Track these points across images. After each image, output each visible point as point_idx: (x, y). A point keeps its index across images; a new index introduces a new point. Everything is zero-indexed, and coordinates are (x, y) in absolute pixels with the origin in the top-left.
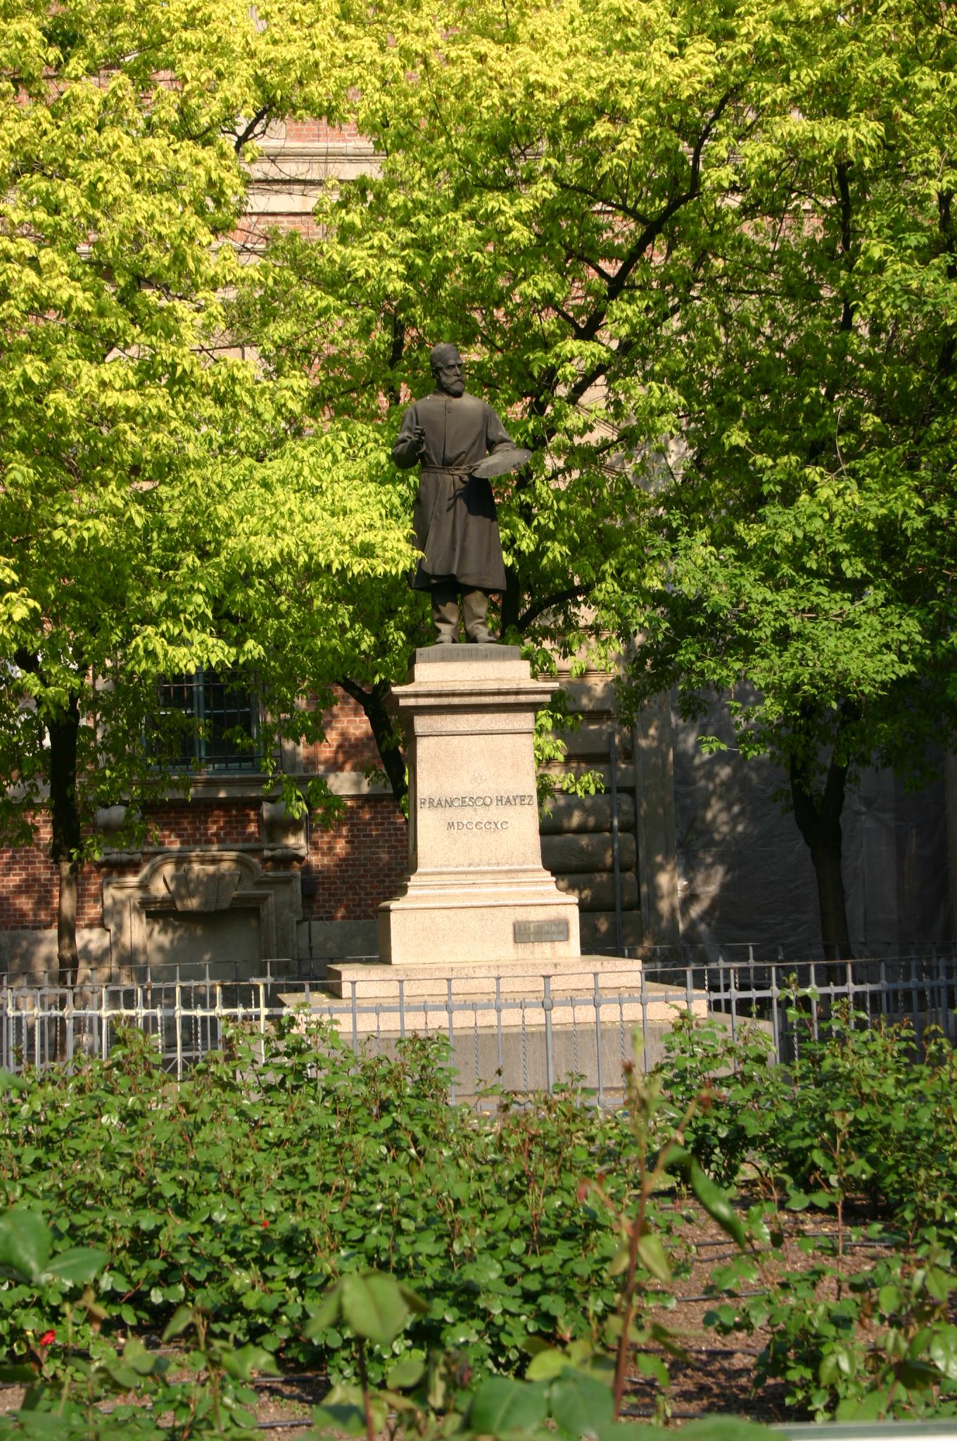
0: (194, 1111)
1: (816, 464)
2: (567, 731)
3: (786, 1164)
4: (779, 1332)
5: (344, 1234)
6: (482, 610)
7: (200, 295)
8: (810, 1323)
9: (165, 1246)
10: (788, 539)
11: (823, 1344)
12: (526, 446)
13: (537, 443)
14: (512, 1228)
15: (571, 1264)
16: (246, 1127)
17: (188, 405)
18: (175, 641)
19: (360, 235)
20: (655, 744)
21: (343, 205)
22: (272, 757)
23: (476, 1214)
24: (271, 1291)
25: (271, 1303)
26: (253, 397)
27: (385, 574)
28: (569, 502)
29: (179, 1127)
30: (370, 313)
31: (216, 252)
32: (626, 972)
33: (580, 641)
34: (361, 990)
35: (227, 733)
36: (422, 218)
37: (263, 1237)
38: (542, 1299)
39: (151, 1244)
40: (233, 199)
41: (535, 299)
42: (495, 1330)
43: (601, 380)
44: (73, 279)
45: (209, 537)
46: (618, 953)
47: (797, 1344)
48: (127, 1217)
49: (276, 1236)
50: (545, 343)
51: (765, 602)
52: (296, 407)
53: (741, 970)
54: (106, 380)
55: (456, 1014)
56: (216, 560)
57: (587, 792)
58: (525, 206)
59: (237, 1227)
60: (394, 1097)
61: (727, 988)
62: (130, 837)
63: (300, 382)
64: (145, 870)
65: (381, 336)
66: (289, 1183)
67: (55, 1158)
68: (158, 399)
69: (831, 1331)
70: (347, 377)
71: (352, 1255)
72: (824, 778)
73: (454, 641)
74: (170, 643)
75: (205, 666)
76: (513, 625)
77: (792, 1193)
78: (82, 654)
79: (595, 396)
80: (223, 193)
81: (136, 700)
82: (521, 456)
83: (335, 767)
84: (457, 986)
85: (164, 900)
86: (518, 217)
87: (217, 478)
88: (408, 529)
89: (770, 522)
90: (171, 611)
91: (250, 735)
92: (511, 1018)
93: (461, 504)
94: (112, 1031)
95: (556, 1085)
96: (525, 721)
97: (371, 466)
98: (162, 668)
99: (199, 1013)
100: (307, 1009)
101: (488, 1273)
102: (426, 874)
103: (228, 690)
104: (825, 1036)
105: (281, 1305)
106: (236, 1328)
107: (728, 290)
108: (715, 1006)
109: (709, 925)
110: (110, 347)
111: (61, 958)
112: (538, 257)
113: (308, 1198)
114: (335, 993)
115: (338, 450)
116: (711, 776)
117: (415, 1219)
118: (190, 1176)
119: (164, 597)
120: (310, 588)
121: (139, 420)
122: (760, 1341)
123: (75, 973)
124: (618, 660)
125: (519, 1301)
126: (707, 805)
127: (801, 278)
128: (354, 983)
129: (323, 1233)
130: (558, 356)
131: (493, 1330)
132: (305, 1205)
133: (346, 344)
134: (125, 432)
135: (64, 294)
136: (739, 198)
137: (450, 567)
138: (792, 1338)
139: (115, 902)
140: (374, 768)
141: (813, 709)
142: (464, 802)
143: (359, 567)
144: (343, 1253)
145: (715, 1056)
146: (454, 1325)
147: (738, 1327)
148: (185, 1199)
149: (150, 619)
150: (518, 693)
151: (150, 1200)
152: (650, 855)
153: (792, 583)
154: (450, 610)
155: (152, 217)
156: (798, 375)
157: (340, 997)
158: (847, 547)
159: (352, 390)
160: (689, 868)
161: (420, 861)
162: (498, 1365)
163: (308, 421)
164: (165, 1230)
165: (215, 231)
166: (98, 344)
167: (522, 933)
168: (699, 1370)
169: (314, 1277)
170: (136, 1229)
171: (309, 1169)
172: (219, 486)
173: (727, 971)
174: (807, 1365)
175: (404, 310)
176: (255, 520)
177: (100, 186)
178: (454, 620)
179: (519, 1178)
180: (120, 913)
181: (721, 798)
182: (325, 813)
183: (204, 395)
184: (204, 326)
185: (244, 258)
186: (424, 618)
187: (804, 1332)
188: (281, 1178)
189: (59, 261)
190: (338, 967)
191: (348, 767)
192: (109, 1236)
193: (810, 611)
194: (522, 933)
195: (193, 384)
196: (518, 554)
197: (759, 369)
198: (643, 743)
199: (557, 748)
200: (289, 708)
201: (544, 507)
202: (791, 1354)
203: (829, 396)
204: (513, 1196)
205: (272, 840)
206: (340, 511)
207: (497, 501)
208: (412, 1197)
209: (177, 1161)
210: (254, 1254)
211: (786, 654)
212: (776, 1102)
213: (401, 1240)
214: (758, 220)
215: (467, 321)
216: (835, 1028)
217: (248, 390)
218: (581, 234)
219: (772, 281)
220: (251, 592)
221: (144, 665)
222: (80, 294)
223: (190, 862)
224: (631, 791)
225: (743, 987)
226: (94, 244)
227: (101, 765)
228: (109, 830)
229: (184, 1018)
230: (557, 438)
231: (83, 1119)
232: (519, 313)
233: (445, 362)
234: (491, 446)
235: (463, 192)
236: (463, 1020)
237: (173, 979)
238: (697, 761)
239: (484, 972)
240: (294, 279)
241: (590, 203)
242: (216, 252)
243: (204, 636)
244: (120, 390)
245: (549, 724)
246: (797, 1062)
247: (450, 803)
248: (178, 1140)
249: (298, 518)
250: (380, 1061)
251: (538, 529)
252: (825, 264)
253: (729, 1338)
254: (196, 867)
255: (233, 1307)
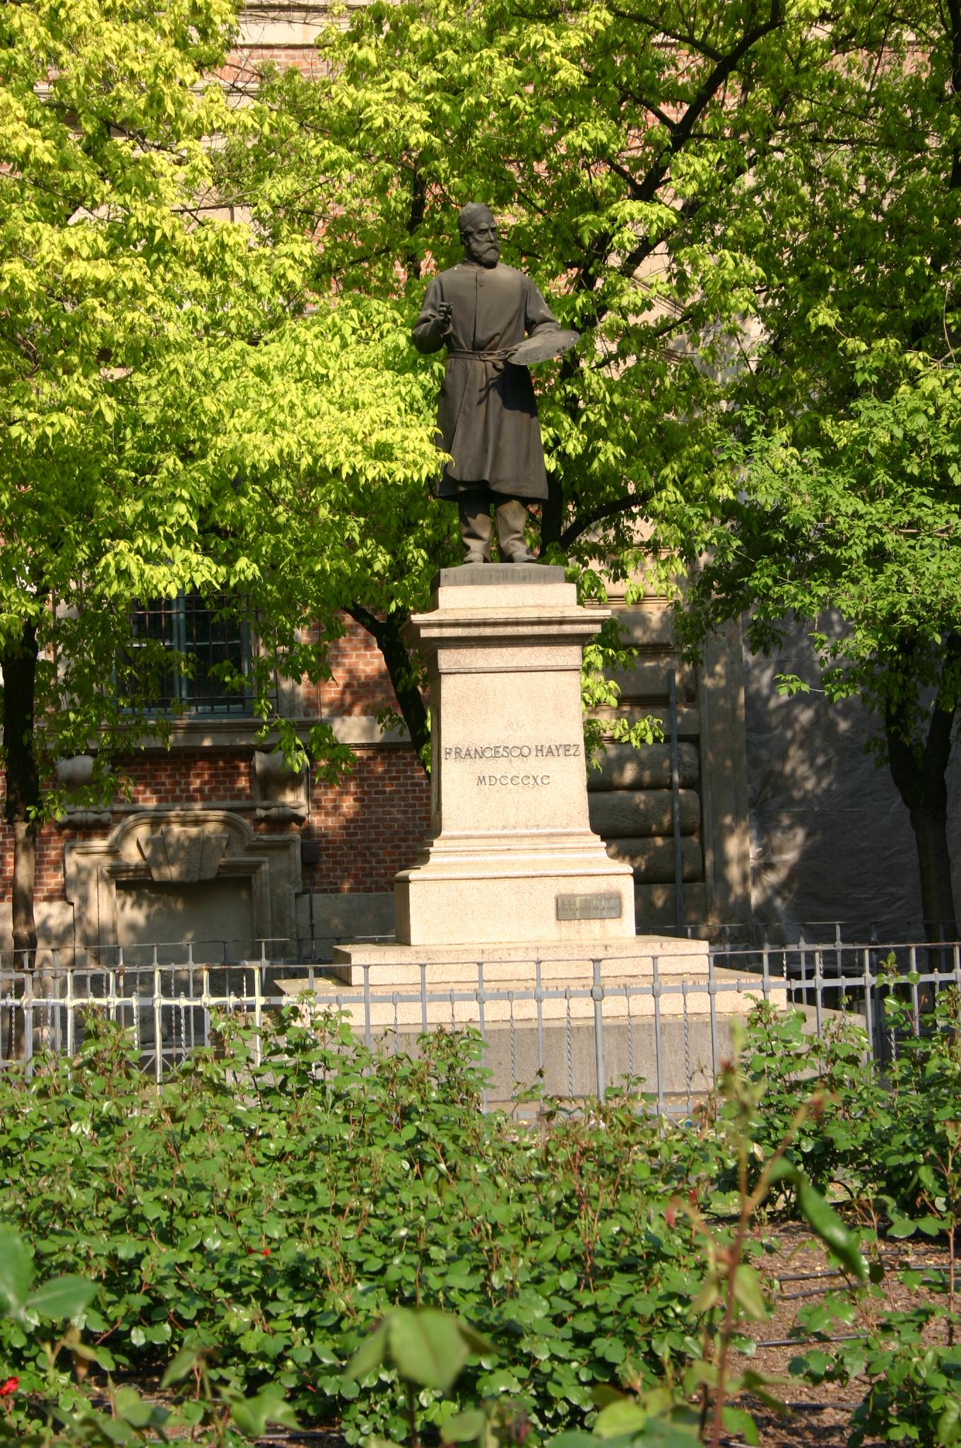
0: (182, 1119)
1: (919, 349)
2: (620, 668)
3: (883, 1184)
4: (879, 1382)
5: (359, 1265)
6: (519, 522)
7: (182, 144)
8: (917, 1371)
9: (148, 1278)
10: (886, 440)
11: (932, 1397)
12: (573, 326)
13: (587, 323)
14: (561, 1258)
15: (631, 1301)
16: (241, 1137)
17: (169, 276)
18: (152, 558)
19: (375, 72)
20: (723, 683)
21: (355, 37)
22: (268, 698)
23: (518, 1242)
24: (275, 1332)
25: (274, 1346)
26: (246, 267)
27: (406, 479)
28: (624, 394)
29: (164, 1138)
30: (387, 168)
31: (202, 93)
32: (690, 955)
33: (636, 560)
34: (376, 975)
35: (214, 669)
36: (450, 54)
37: (264, 1268)
38: (596, 1343)
39: (131, 1275)
40: (221, 29)
41: (584, 152)
42: (540, 1379)
43: (662, 247)
44: (31, 126)
45: (193, 434)
46: (679, 933)
47: (901, 1398)
48: (102, 1244)
49: (279, 1267)
50: (595, 203)
51: (856, 515)
52: (296, 276)
53: (825, 954)
54: (70, 247)
55: (488, 1004)
56: (202, 462)
57: (643, 741)
58: (575, 40)
59: (233, 1256)
60: (417, 1103)
61: (810, 974)
62: (99, 792)
63: (305, 247)
64: (115, 833)
65: (399, 195)
66: (293, 1204)
67: (15, 1174)
68: (133, 271)
69: (941, 1382)
70: (357, 243)
71: (370, 1290)
72: (926, 725)
73: (485, 561)
74: (147, 561)
75: (188, 588)
76: (555, 542)
77: (894, 1217)
78: (42, 574)
79: (655, 267)
80: (210, 21)
81: (105, 629)
82: (567, 339)
83: (342, 710)
84: (490, 972)
85: (137, 868)
86: (564, 54)
87: (202, 365)
88: (433, 429)
89: (863, 418)
90: (149, 523)
91: (241, 672)
92: (554, 1009)
93: (494, 396)
94: (79, 1025)
95: (608, 1089)
96: (570, 656)
97: (387, 351)
98: (137, 590)
99: (182, 1002)
100: (310, 997)
101: (532, 1311)
102: (452, 838)
103: (216, 619)
104: (927, 1034)
105: (287, 1348)
106: (234, 1374)
107: (815, 139)
108: (794, 996)
109: (784, 899)
110: (75, 206)
111: (16, 937)
112: (589, 100)
113: (317, 1222)
114: (343, 979)
115: (347, 331)
116: (789, 721)
117: (445, 1247)
118: (177, 1195)
119: (140, 506)
120: (316, 493)
121: (111, 295)
122: (856, 1394)
123: (33, 954)
124: (679, 580)
125: (570, 1345)
126: (784, 757)
127: (903, 123)
128: (366, 967)
129: (335, 1264)
130: (613, 220)
131: (539, 1379)
132: (313, 1229)
133: (355, 204)
134: (94, 310)
135: (21, 144)
136: (829, 27)
137: (481, 472)
138: (894, 1390)
139: (80, 869)
140: (389, 711)
141: (913, 643)
142: (497, 752)
143: (373, 471)
144: (360, 1287)
145: (799, 1056)
146: (491, 1372)
147: (830, 1377)
148: (170, 1223)
149: (123, 532)
150: (561, 622)
151: (129, 1223)
152: (718, 814)
153: (889, 491)
154: (481, 523)
155: (126, 49)
156: (899, 242)
157: (348, 984)
158: (955, 449)
159: (362, 260)
160: (765, 828)
161: (446, 822)
162: (544, 1420)
163: (311, 296)
164: (147, 1258)
165: (199, 68)
166: (60, 204)
167: (566, 909)
168: (782, 1428)
169: (326, 1315)
170: (113, 1257)
171: (319, 1187)
172: (205, 374)
173: (810, 956)
174: (912, 1423)
175: (424, 163)
176: (248, 414)
177: (62, 13)
178: (486, 534)
179: (568, 1199)
180: (85, 884)
181: (801, 746)
182: (332, 764)
183: (188, 265)
184: (187, 182)
185: (233, 100)
186: (449, 533)
187: (909, 1382)
188: (284, 1197)
189: (15, 104)
190: (346, 948)
191: (357, 710)
192: (82, 1265)
193: (910, 525)
194: (566, 909)
195: (175, 252)
196: (563, 457)
197: (851, 234)
198: (708, 682)
199: (609, 691)
200: (288, 640)
201: (592, 400)
202: (893, 1410)
203: (935, 266)
204: (560, 1221)
205: (265, 798)
206: (350, 404)
207: (537, 392)
208: (440, 1220)
209: (161, 1177)
210: (252, 1288)
211: (881, 577)
212: (873, 1110)
213: (429, 1272)
214: (851, 54)
215: (499, 176)
216: (941, 1023)
217: (240, 259)
218: (640, 71)
219: (867, 129)
220: (244, 501)
221: (115, 587)
222: (39, 143)
223: (169, 823)
224: (694, 740)
225: (828, 974)
226: (54, 83)
227: (64, 707)
228: (73, 784)
229: (166, 1009)
230: (609, 317)
231: (49, 1128)
232: (564, 167)
233: (475, 225)
234: (530, 326)
235: (497, 23)
236: (496, 1012)
237: (150, 962)
238: (773, 704)
239: (520, 955)
240: (294, 126)
241: (650, 34)
242: (202, 93)
243: (187, 553)
244: (88, 259)
245: (599, 661)
246: (895, 1064)
247: (480, 754)
248: (162, 1154)
249: (300, 413)
250: (400, 1060)
251: (587, 427)
252: (930, 107)
253: (817, 1389)
254: (176, 829)
255: (229, 1351)
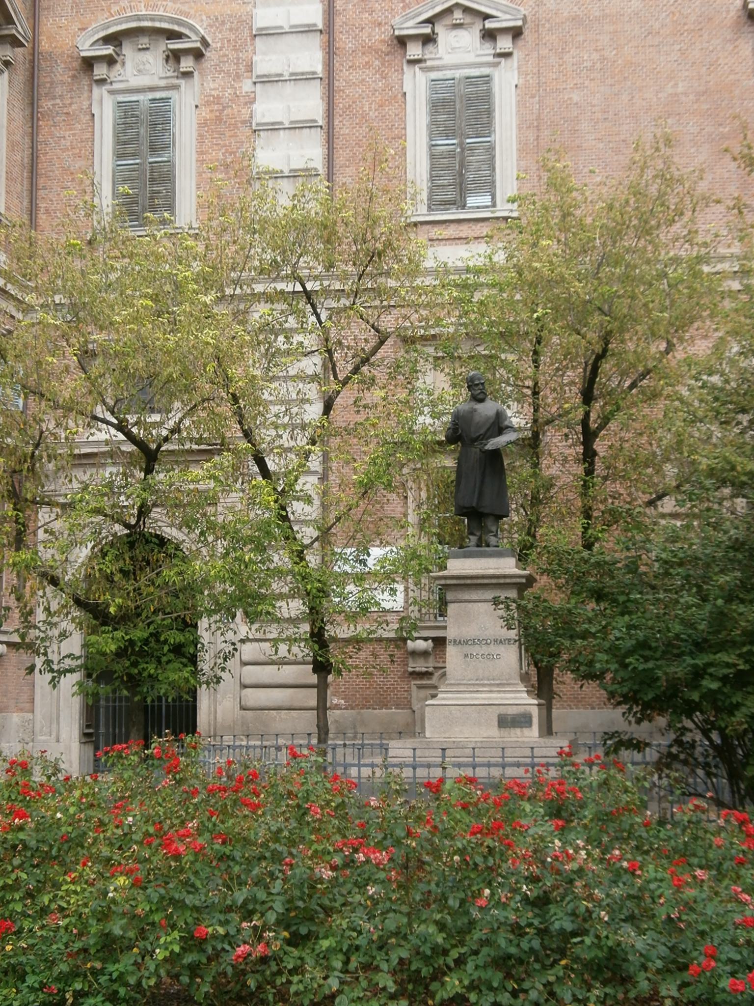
55: (418, 770)
142: (474, 642)
167: (505, 722)
194: (505, 722)
247: (466, 642)
